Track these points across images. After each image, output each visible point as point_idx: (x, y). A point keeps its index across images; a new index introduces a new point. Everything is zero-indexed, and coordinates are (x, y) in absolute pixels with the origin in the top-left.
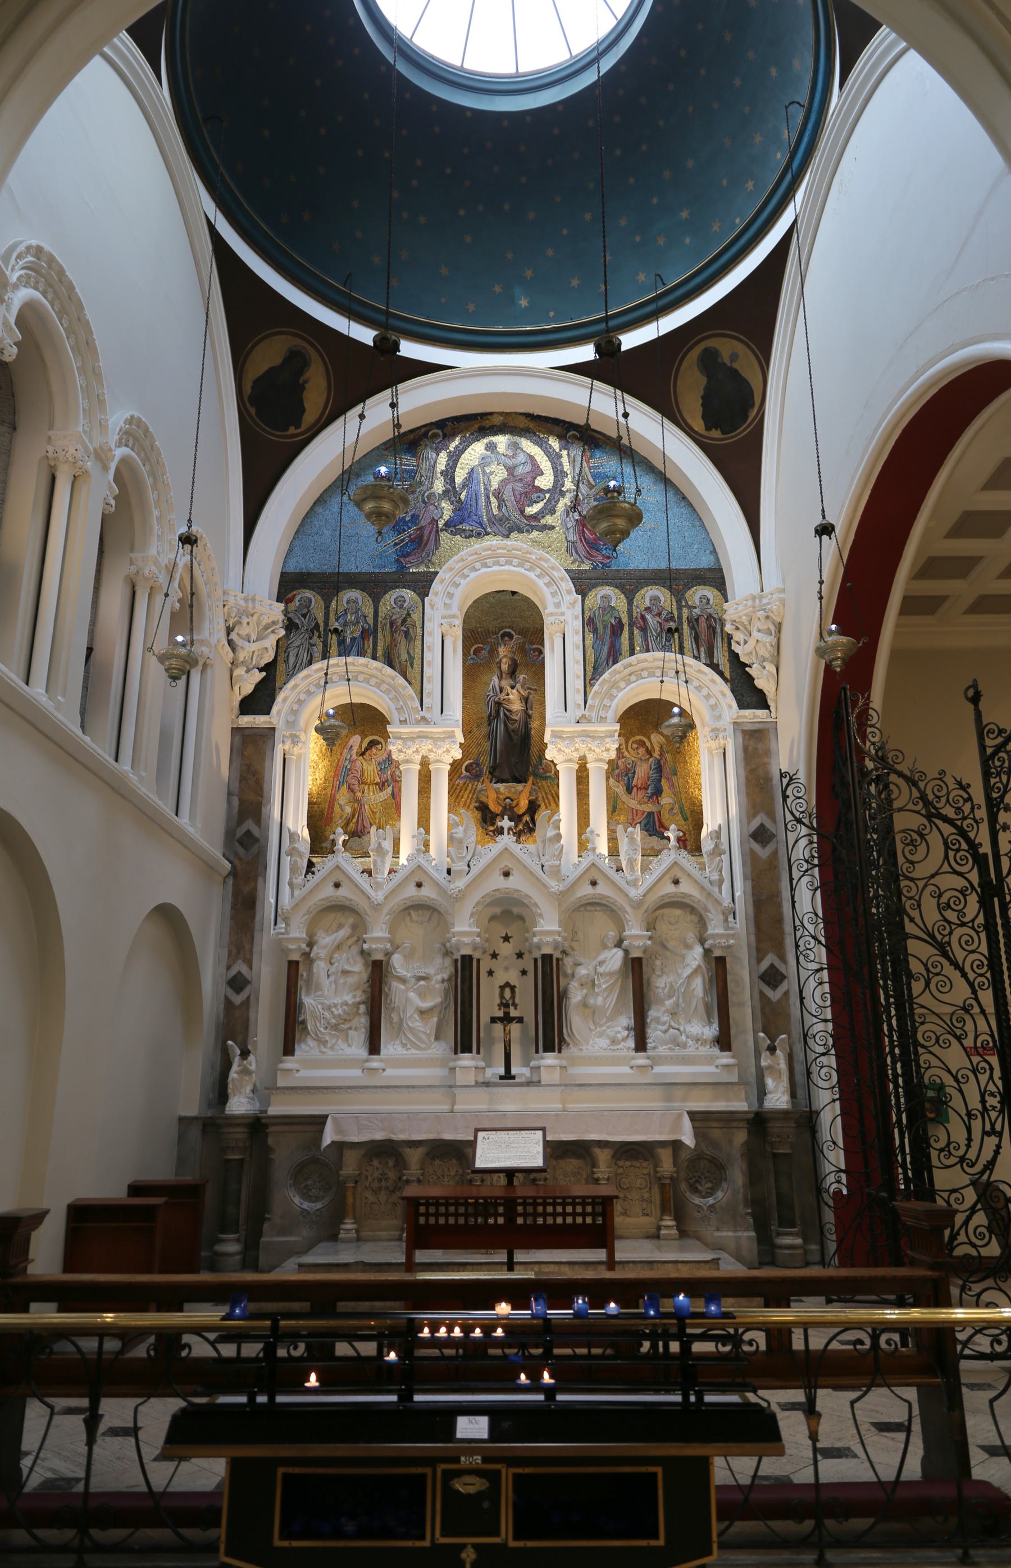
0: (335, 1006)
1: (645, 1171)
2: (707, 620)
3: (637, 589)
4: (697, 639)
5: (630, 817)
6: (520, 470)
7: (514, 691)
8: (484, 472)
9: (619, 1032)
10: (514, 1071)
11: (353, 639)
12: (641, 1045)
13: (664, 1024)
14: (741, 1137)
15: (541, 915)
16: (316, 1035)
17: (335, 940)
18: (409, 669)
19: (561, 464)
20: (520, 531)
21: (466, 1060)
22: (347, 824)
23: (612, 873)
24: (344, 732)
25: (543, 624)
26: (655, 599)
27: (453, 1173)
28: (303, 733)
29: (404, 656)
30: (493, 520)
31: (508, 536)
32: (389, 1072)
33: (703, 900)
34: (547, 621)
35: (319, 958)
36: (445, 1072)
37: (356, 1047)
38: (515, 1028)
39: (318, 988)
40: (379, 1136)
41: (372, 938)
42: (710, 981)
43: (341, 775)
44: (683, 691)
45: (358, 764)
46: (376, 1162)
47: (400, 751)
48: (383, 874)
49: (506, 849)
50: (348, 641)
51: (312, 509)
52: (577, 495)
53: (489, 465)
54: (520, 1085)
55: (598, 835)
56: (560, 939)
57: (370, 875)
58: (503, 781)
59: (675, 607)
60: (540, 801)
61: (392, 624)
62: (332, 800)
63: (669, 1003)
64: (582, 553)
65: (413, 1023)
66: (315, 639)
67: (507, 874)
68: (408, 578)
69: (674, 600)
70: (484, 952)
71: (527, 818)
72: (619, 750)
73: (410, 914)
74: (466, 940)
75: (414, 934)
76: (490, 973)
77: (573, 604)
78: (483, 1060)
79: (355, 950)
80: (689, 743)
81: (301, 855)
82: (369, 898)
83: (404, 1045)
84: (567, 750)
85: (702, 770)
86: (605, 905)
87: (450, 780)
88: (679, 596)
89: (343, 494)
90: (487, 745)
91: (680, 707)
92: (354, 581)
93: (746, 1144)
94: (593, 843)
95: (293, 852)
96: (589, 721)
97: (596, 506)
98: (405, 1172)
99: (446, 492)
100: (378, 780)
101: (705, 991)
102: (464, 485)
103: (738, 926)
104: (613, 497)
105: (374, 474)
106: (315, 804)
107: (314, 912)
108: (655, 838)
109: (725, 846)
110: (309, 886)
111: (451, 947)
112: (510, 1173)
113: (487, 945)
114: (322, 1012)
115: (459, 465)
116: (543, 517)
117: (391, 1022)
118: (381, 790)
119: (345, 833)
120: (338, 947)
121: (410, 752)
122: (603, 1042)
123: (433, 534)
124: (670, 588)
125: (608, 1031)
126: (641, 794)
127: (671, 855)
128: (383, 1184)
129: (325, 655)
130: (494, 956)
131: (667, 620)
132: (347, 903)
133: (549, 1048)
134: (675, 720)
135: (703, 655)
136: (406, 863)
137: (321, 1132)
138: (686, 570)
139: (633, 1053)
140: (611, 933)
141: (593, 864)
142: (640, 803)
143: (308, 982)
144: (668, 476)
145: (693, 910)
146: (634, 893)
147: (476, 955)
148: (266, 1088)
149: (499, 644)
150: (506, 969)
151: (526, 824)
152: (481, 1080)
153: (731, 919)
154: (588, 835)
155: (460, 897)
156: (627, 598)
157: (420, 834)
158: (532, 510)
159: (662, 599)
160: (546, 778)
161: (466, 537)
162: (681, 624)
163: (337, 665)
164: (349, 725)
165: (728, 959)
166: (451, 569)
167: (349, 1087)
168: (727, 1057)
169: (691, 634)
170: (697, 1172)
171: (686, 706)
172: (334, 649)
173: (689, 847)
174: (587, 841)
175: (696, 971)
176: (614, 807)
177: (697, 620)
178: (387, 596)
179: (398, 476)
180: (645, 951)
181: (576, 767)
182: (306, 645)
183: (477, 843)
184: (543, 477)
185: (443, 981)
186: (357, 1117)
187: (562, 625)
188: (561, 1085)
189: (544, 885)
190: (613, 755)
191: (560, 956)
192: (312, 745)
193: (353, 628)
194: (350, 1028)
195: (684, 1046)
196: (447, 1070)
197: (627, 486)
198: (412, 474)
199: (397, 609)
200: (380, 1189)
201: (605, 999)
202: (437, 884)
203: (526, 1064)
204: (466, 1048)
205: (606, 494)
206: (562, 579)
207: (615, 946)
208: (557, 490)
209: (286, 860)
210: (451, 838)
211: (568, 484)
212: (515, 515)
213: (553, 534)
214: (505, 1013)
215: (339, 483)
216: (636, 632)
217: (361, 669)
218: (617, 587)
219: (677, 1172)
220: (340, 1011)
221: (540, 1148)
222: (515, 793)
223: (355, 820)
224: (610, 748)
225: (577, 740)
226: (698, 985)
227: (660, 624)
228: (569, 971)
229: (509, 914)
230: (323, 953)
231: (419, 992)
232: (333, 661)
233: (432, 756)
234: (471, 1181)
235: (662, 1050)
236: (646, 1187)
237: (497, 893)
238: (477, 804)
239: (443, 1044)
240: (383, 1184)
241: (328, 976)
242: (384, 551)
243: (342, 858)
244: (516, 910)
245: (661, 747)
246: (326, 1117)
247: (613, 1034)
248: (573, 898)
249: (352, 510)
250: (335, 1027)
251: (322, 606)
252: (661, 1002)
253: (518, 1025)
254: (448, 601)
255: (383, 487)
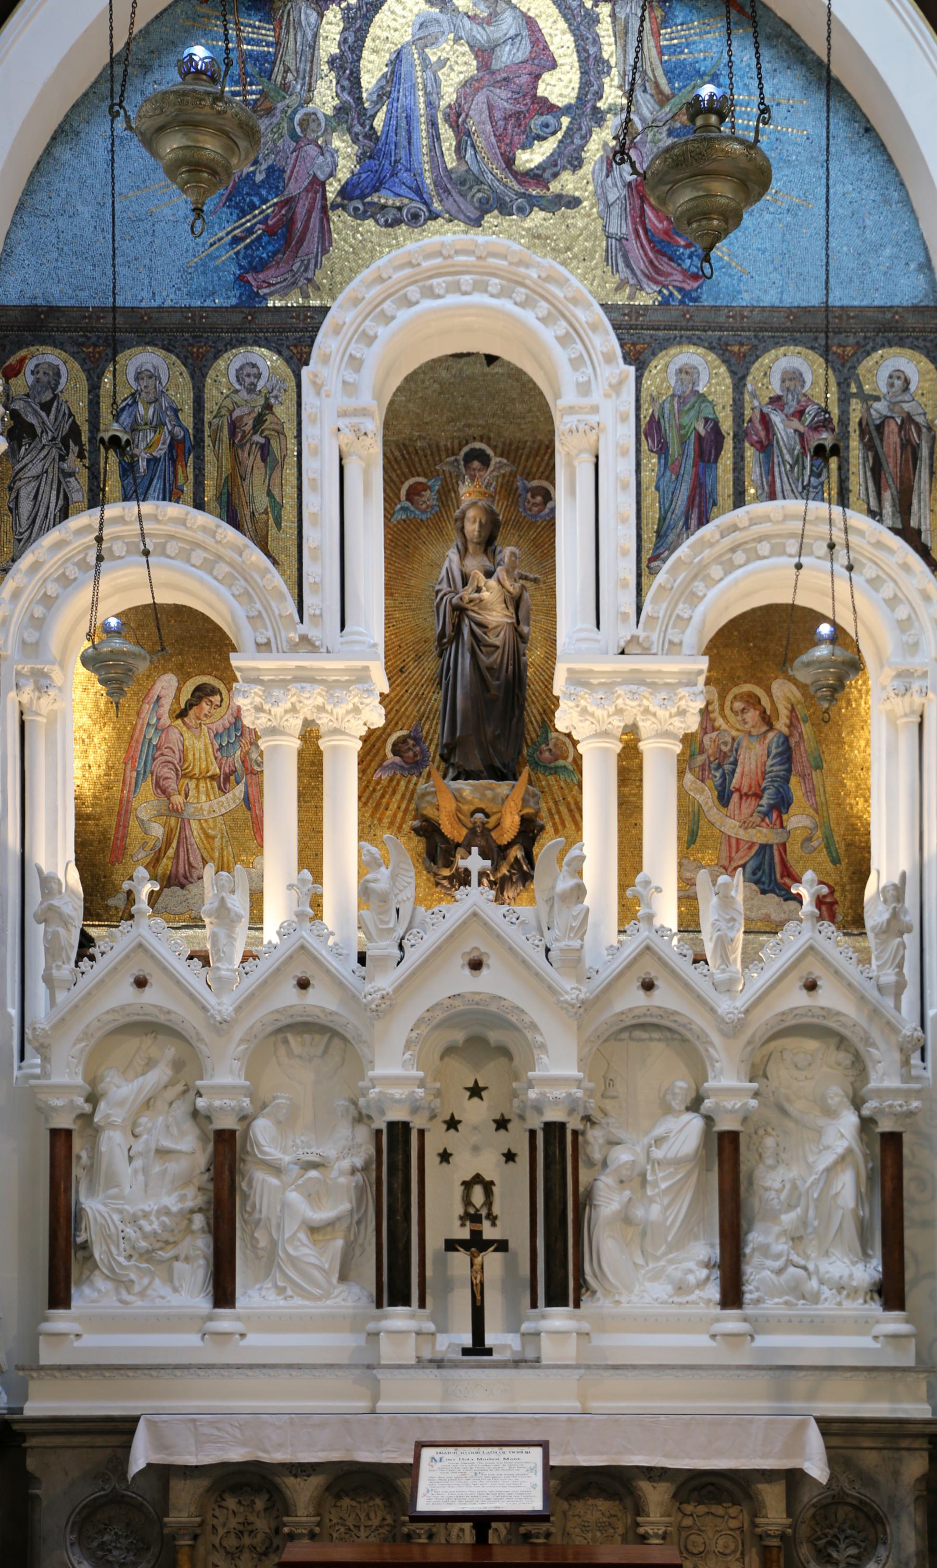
0: (146, 1215)
1: (733, 1524)
2: (901, 427)
3: (755, 354)
4: (877, 471)
5: (725, 854)
6: (506, 56)
7: (492, 582)
8: (425, 59)
9: (691, 1271)
10: (490, 1340)
11: (153, 462)
12: (732, 1295)
13: (778, 1256)
14: (915, 1466)
15: (543, 1047)
16: (112, 1270)
17: (140, 1090)
18: (273, 531)
19: (596, 41)
20: (504, 209)
21: (399, 1319)
22: (156, 861)
23: (685, 967)
24: (142, 667)
25: (552, 432)
26: (793, 378)
27: (376, 1522)
28: (56, 668)
29: (262, 502)
30: (449, 183)
31: (477, 222)
32: (253, 1339)
33: (863, 1022)
34: (562, 424)
35: (112, 1125)
36: (359, 1340)
37: (190, 1293)
38: (492, 1261)
39: (112, 1181)
40: (237, 1455)
41: (212, 1087)
42: (870, 1178)
43: (139, 758)
44: (842, 586)
45: (174, 735)
46: (231, 1502)
47: (259, 709)
48: (231, 961)
49: (475, 914)
50: (142, 465)
51: (48, 151)
52: (628, 120)
53: (435, 42)
54: (503, 1365)
55: (659, 890)
56: (580, 1094)
57: (206, 963)
58: (468, 775)
59: (833, 396)
60: (544, 819)
61: (234, 427)
62: (124, 811)
63: (789, 1218)
64: (640, 264)
65: (296, 1248)
66: (73, 462)
67: (476, 965)
68: (265, 320)
69: (832, 380)
70: (433, 1117)
71: (517, 852)
72: (705, 713)
73: (286, 1041)
74: (398, 1093)
75: (296, 1078)
76: (445, 1157)
77: (616, 388)
78: (432, 1318)
79: (181, 1109)
80: (849, 703)
81: (65, 922)
82: (204, 1009)
83: (281, 1291)
84: (599, 713)
85: (873, 759)
86: (670, 1030)
87: (362, 772)
88: (844, 370)
89: (114, 115)
90: (436, 699)
91: (833, 623)
92: (148, 327)
93: (925, 1479)
94: (649, 906)
95: (50, 915)
96: (646, 651)
97: (668, 150)
98: (285, 1519)
99: (341, 110)
100: (215, 769)
101: (859, 1196)
102: (383, 94)
103: (929, 1074)
104: (706, 127)
105: (180, 63)
106: (88, 817)
107: (99, 1034)
108: (772, 899)
109: (912, 917)
110: (85, 983)
111: (368, 1105)
112: (481, 1522)
113: (437, 1102)
114: (121, 1226)
115: (368, 43)
116: (555, 175)
117: (254, 1247)
118: (223, 790)
119: (154, 877)
120: (148, 1104)
121: (278, 710)
122: (661, 1290)
123: (316, 215)
124: (826, 353)
125: (670, 1269)
126: (748, 806)
127: (804, 932)
128: (247, 1540)
129: (96, 499)
130: (452, 1124)
131: (815, 428)
132: (162, 1019)
133: (556, 1298)
134: (822, 651)
135: (888, 509)
136: (276, 940)
137: (127, 1447)
138: (862, 309)
139: (717, 1311)
140: (681, 1084)
141: (648, 948)
142: (745, 825)
143: (92, 1169)
144: (835, 71)
145: (842, 1041)
146: (727, 1006)
147: (417, 1123)
148: (18, 1368)
149: (459, 477)
150: (476, 1149)
151: (515, 862)
152: (427, 1354)
153: (915, 1059)
154: (639, 888)
155: (385, 1008)
156: (733, 373)
157: (303, 881)
158: (531, 158)
159: (808, 377)
160: (556, 771)
161: (387, 225)
162: (845, 436)
163: (121, 520)
164: (152, 653)
165: (906, 1138)
166: (356, 301)
167: (177, 1367)
168: (895, 1321)
169: (866, 459)
170: (831, 1526)
171: (846, 621)
172: (113, 485)
173: (839, 918)
174: (637, 900)
175: (842, 1159)
176: (692, 833)
177: (880, 428)
178: (221, 363)
179: (235, 70)
180: (745, 1120)
181: (618, 747)
182: (53, 474)
183: (418, 901)
184: (556, 73)
185: (353, 1171)
186: (194, 1421)
187: (592, 436)
188: (577, 1367)
189: (550, 987)
190: (693, 724)
191: (579, 1126)
192: (77, 694)
193: (151, 436)
194: (177, 1258)
195: (816, 1298)
196: (364, 1336)
197: (740, 96)
198: (264, 65)
199: (244, 394)
200: (240, 1549)
201: (666, 1208)
202: (339, 983)
203: (513, 1326)
204: (399, 1297)
205: (692, 119)
206: (594, 327)
207: (688, 1109)
208: (586, 108)
209: (37, 933)
210: (365, 892)
211: (612, 94)
212: (494, 172)
213: (578, 219)
214: (472, 1232)
215: (105, 89)
216: (750, 453)
217: (171, 528)
218: (711, 348)
219: (793, 1526)
220: (156, 1226)
221: (538, 1479)
222: (493, 800)
223: (171, 852)
224: (685, 711)
225: (620, 690)
226: (846, 1187)
227: (802, 436)
228: (597, 1156)
229: (481, 1043)
230: (118, 1116)
231: (307, 1192)
232: (112, 510)
233: (324, 721)
234: (409, 1537)
235: (773, 1306)
236: (734, 1552)
237: (457, 1002)
238: (416, 823)
239: (356, 1290)
240: (247, 1540)
241: (131, 1159)
242: (211, 257)
243: (147, 928)
244: (494, 1036)
245: (793, 710)
246: (135, 1420)
247: (678, 1275)
248: (606, 1015)
249: (134, 154)
250: (147, 1255)
251: (83, 385)
252: (774, 1217)
253: (499, 1255)
254: (351, 377)
255: (199, 97)
